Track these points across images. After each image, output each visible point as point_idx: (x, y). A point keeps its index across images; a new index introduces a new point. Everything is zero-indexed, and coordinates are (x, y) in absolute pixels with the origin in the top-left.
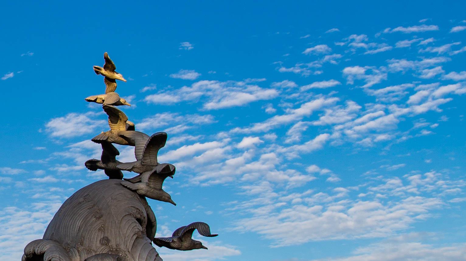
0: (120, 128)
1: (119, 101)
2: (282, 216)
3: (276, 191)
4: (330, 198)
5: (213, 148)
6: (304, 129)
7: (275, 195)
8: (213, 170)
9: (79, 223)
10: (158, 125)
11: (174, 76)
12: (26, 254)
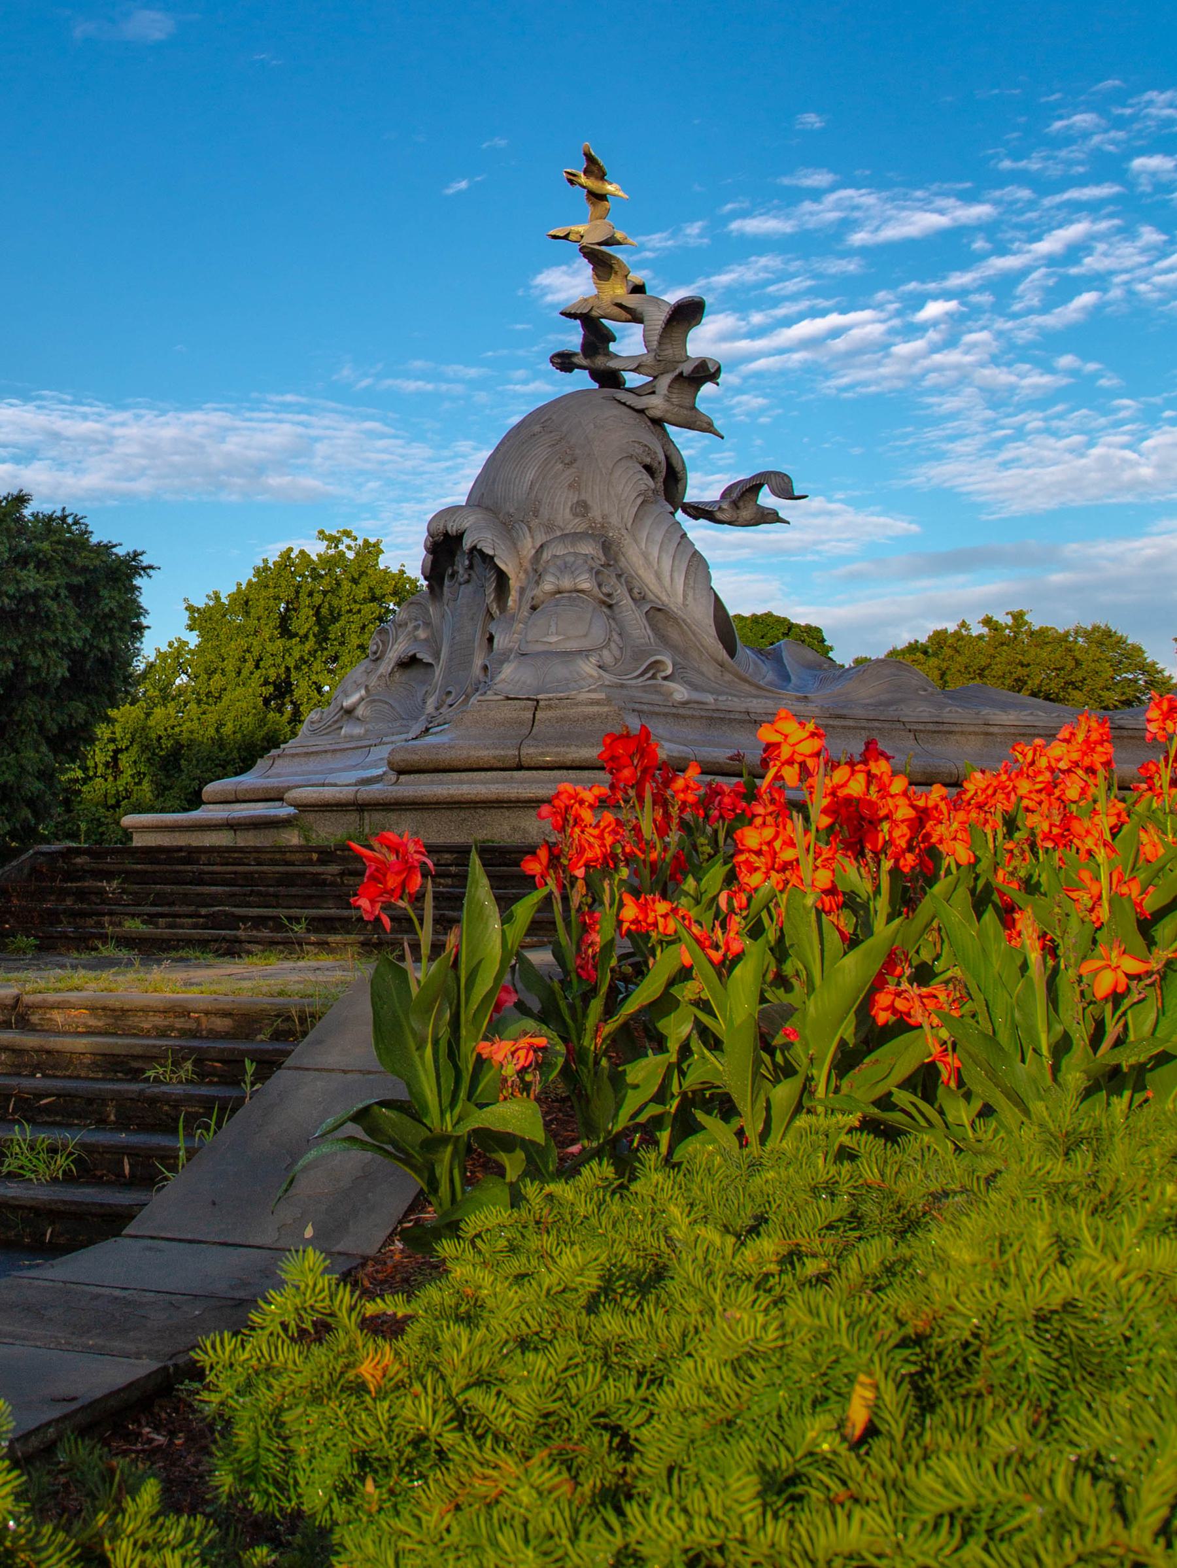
0: (618, 290)
1: (613, 237)
2: (1005, 455)
3: (994, 405)
4: (1102, 421)
5: (864, 324)
6: (1051, 282)
7: (989, 414)
8: (862, 366)
9: (530, 475)
10: (754, 278)
11: (786, 181)
12: (431, 535)
